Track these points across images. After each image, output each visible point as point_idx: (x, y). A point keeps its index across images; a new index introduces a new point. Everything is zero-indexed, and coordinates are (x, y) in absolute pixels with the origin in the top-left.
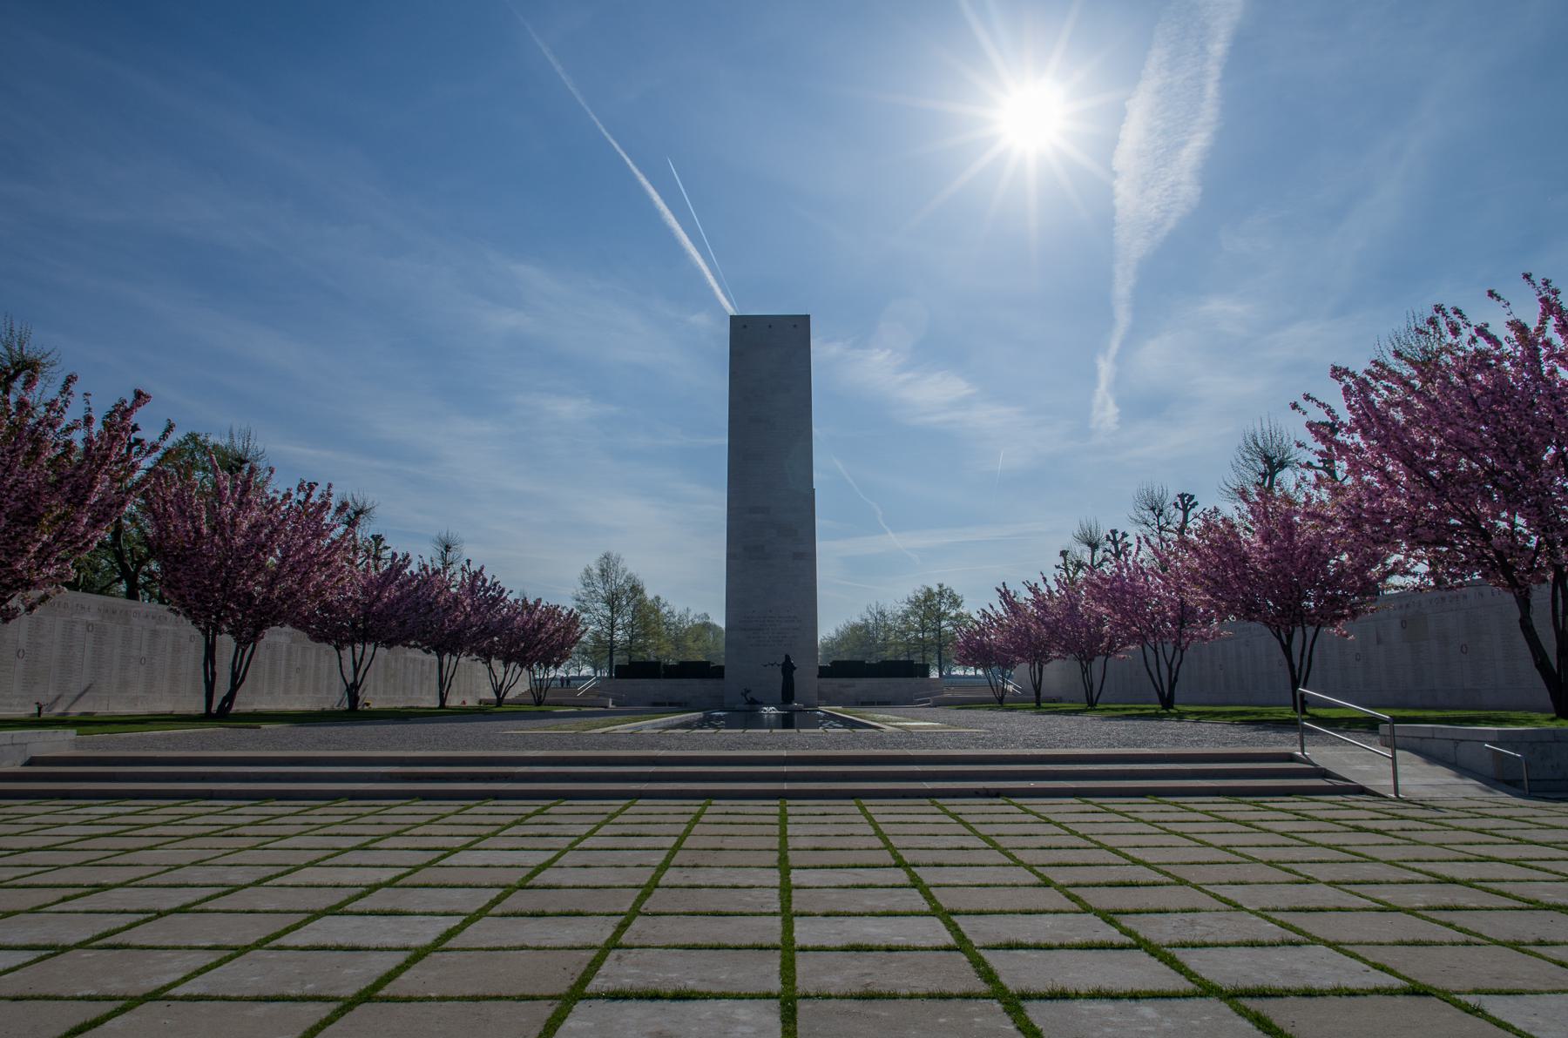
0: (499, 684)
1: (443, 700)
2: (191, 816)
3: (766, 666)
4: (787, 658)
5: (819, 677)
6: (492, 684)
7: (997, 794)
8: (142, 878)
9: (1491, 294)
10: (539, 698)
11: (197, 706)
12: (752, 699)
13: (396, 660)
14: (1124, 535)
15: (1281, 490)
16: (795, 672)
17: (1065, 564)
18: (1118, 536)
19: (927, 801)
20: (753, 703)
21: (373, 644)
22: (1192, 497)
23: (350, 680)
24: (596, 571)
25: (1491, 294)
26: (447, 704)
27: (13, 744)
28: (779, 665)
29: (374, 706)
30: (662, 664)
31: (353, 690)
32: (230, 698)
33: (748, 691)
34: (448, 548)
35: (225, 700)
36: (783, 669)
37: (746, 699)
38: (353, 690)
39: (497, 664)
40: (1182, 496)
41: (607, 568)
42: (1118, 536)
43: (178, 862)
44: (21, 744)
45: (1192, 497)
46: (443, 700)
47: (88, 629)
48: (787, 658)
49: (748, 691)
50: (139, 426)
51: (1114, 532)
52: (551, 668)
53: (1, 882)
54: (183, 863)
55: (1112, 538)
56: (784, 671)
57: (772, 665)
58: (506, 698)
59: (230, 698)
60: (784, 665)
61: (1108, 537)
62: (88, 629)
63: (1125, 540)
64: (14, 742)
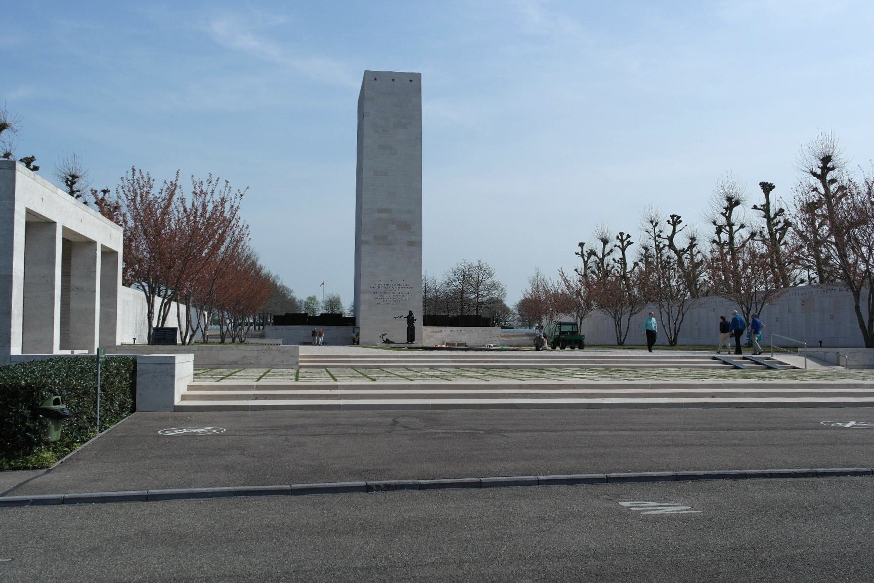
4: (411, 313)
14: (628, 236)
17: (582, 252)
18: (624, 237)
20: (389, 343)
33: (385, 334)
40: (673, 216)
42: (624, 237)
45: (679, 217)
48: (411, 313)
49: (385, 334)
51: (622, 234)
55: (620, 238)
56: (408, 322)
60: (408, 318)
63: (629, 239)
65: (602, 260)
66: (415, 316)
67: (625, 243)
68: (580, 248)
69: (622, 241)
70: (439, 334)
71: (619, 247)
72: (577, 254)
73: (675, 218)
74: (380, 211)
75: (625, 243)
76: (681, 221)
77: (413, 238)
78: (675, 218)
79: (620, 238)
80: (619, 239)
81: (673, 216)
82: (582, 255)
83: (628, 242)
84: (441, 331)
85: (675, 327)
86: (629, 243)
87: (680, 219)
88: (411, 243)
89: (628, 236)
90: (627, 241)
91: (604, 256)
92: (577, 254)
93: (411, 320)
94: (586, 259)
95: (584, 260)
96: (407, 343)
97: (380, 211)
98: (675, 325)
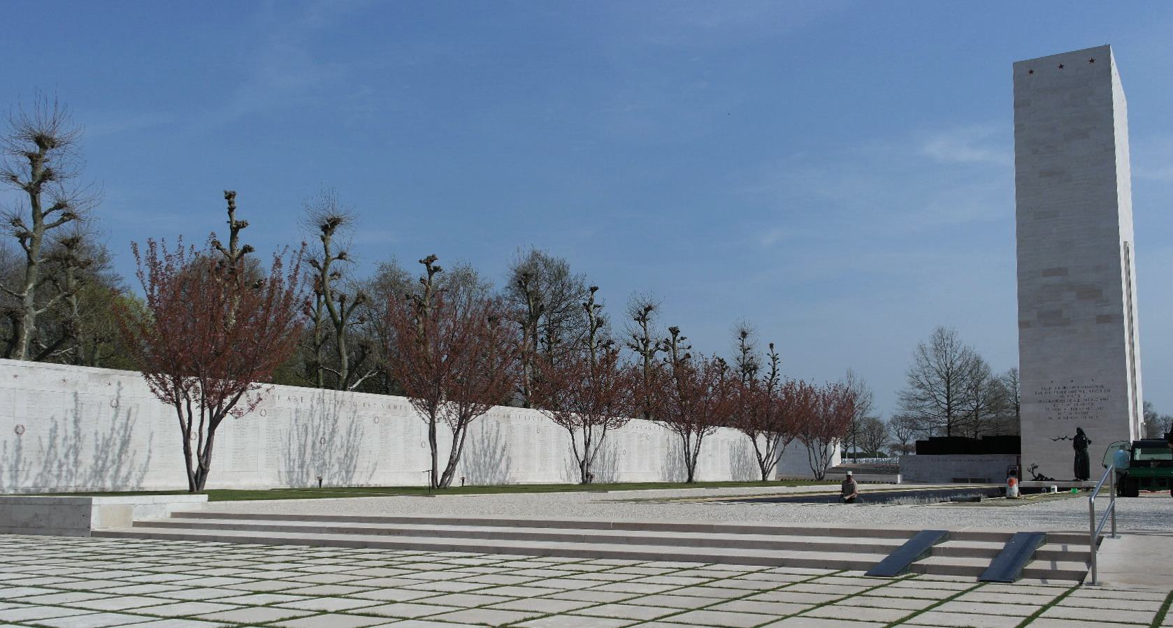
2: (518, 569)
4: (1080, 432)
7: (182, 537)
8: (282, 602)
9: (230, 196)
10: (820, 474)
11: (425, 481)
16: (1089, 447)
19: (1038, 582)
21: (1075, 478)
24: (930, 345)
25: (230, 196)
26: (694, 478)
27: (154, 504)
28: (1070, 439)
29: (699, 480)
32: (449, 472)
33: (1036, 467)
34: (744, 334)
35: (445, 474)
36: (1075, 443)
37: (1034, 476)
41: (942, 343)
43: (549, 611)
44: (161, 504)
47: (374, 420)
48: (1080, 432)
50: (437, 257)
53: (2, 580)
54: (397, 600)
56: (1076, 446)
57: (1063, 439)
59: (449, 472)
60: (1076, 438)
62: (374, 420)
64: (155, 502)
66: (1089, 434)
74: (1047, 273)
77: (1107, 310)
97: (1047, 273)
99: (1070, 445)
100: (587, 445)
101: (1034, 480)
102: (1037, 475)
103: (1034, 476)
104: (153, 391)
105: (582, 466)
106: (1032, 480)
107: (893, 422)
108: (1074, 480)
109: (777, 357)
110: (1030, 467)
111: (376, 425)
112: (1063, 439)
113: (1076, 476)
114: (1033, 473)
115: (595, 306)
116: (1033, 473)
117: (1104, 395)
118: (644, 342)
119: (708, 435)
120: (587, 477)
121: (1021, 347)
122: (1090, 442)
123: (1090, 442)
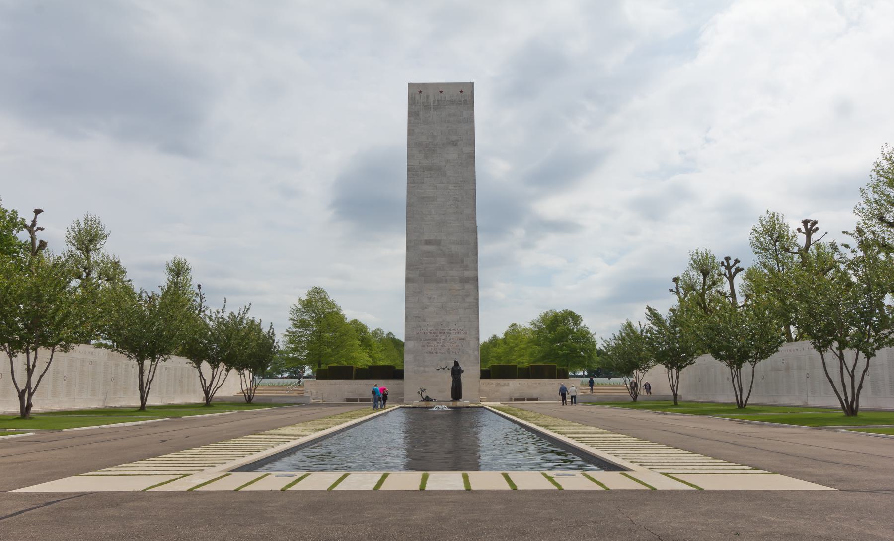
0: (207, 386)
1: (143, 400)
3: (438, 370)
4: (456, 363)
5: (481, 378)
6: (203, 386)
12: (427, 397)
13: (117, 366)
14: (737, 261)
15: (795, 241)
17: (677, 288)
18: (731, 263)
20: (428, 401)
21: (452, 399)
22: (815, 222)
23: (22, 387)
28: (449, 369)
30: (354, 369)
31: (25, 395)
33: (425, 390)
37: (422, 398)
38: (25, 395)
39: (205, 365)
40: (805, 222)
42: (731, 263)
45: (815, 222)
46: (143, 400)
48: (456, 363)
49: (425, 390)
51: (727, 259)
52: (157, 356)
55: (726, 264)
57: (444, 369)
58: (214, 396)
60: (453, 369)
61: (723, 263)
63: (737, 265)
65: (702, 295)
66: (462, 366)
67: (733, 270)
68: (674, 284)
69: (728, 268)
70: (506, 388)
71: (725, 275)
72: (671, 290)
73: (809, 225)
74: (428, 243)
75: (733, 270)
76: (817, 229)
77: (468, 274)
78: (809, 225)
79: (726, 264)
80: (725, 266)
81: (805, 222)
82: (678, 292)
83: (736, 269)
84: (508, 385)
85: (245, 394)
86: (738, 270)
87: (816, 226)
88: (464, 280)
89: (737, 261)
90: (734, 268)
91: (704, 290)
92: (671, 290)
93: (457, 372)
94: (683, 296)
95: (680, 297)
96: (53, 352)
98: (852, 377)
99: (449, 373)
100: (30, 371)
101: (423, 401)
102: (424, 398)
103: (422, 398)
104: (868, 467)
105: (21, 395)
106: (421, 401)
107: (646, 360)
108: (53, 352)
109: (203, 296)
110: (420, 391)
111: (808, 379)
112: (444, 369)
113: (452, 398)
114: (421, 395)
115: (38, 229)
116: (421, 395)
117: (462, 336)
118: (87, 271)
119: (162, 360)
120: (26, 410)
121: (407, 297)
122: (463, 371)
123: (463, 371)
